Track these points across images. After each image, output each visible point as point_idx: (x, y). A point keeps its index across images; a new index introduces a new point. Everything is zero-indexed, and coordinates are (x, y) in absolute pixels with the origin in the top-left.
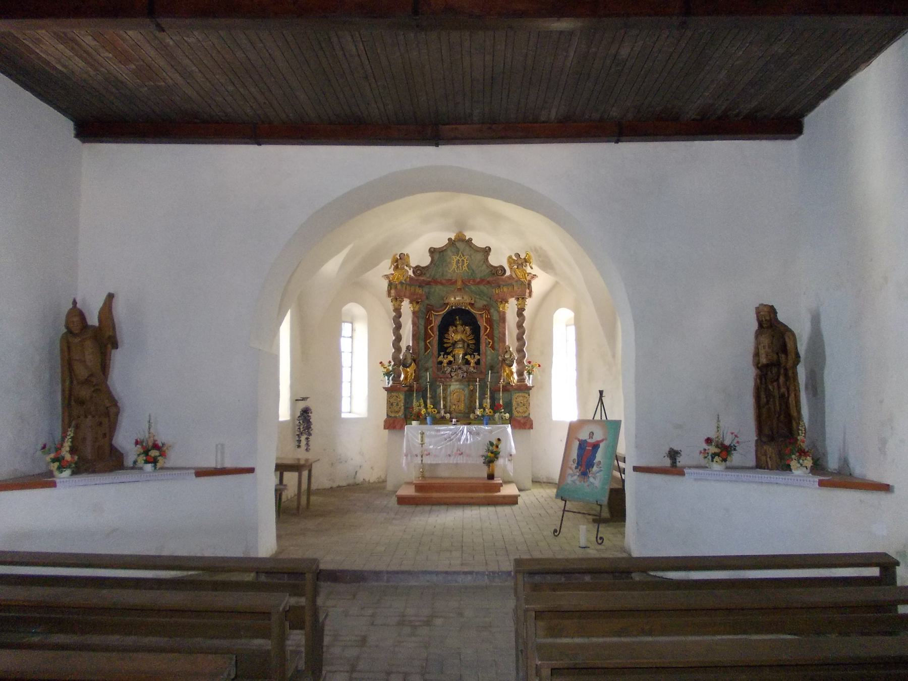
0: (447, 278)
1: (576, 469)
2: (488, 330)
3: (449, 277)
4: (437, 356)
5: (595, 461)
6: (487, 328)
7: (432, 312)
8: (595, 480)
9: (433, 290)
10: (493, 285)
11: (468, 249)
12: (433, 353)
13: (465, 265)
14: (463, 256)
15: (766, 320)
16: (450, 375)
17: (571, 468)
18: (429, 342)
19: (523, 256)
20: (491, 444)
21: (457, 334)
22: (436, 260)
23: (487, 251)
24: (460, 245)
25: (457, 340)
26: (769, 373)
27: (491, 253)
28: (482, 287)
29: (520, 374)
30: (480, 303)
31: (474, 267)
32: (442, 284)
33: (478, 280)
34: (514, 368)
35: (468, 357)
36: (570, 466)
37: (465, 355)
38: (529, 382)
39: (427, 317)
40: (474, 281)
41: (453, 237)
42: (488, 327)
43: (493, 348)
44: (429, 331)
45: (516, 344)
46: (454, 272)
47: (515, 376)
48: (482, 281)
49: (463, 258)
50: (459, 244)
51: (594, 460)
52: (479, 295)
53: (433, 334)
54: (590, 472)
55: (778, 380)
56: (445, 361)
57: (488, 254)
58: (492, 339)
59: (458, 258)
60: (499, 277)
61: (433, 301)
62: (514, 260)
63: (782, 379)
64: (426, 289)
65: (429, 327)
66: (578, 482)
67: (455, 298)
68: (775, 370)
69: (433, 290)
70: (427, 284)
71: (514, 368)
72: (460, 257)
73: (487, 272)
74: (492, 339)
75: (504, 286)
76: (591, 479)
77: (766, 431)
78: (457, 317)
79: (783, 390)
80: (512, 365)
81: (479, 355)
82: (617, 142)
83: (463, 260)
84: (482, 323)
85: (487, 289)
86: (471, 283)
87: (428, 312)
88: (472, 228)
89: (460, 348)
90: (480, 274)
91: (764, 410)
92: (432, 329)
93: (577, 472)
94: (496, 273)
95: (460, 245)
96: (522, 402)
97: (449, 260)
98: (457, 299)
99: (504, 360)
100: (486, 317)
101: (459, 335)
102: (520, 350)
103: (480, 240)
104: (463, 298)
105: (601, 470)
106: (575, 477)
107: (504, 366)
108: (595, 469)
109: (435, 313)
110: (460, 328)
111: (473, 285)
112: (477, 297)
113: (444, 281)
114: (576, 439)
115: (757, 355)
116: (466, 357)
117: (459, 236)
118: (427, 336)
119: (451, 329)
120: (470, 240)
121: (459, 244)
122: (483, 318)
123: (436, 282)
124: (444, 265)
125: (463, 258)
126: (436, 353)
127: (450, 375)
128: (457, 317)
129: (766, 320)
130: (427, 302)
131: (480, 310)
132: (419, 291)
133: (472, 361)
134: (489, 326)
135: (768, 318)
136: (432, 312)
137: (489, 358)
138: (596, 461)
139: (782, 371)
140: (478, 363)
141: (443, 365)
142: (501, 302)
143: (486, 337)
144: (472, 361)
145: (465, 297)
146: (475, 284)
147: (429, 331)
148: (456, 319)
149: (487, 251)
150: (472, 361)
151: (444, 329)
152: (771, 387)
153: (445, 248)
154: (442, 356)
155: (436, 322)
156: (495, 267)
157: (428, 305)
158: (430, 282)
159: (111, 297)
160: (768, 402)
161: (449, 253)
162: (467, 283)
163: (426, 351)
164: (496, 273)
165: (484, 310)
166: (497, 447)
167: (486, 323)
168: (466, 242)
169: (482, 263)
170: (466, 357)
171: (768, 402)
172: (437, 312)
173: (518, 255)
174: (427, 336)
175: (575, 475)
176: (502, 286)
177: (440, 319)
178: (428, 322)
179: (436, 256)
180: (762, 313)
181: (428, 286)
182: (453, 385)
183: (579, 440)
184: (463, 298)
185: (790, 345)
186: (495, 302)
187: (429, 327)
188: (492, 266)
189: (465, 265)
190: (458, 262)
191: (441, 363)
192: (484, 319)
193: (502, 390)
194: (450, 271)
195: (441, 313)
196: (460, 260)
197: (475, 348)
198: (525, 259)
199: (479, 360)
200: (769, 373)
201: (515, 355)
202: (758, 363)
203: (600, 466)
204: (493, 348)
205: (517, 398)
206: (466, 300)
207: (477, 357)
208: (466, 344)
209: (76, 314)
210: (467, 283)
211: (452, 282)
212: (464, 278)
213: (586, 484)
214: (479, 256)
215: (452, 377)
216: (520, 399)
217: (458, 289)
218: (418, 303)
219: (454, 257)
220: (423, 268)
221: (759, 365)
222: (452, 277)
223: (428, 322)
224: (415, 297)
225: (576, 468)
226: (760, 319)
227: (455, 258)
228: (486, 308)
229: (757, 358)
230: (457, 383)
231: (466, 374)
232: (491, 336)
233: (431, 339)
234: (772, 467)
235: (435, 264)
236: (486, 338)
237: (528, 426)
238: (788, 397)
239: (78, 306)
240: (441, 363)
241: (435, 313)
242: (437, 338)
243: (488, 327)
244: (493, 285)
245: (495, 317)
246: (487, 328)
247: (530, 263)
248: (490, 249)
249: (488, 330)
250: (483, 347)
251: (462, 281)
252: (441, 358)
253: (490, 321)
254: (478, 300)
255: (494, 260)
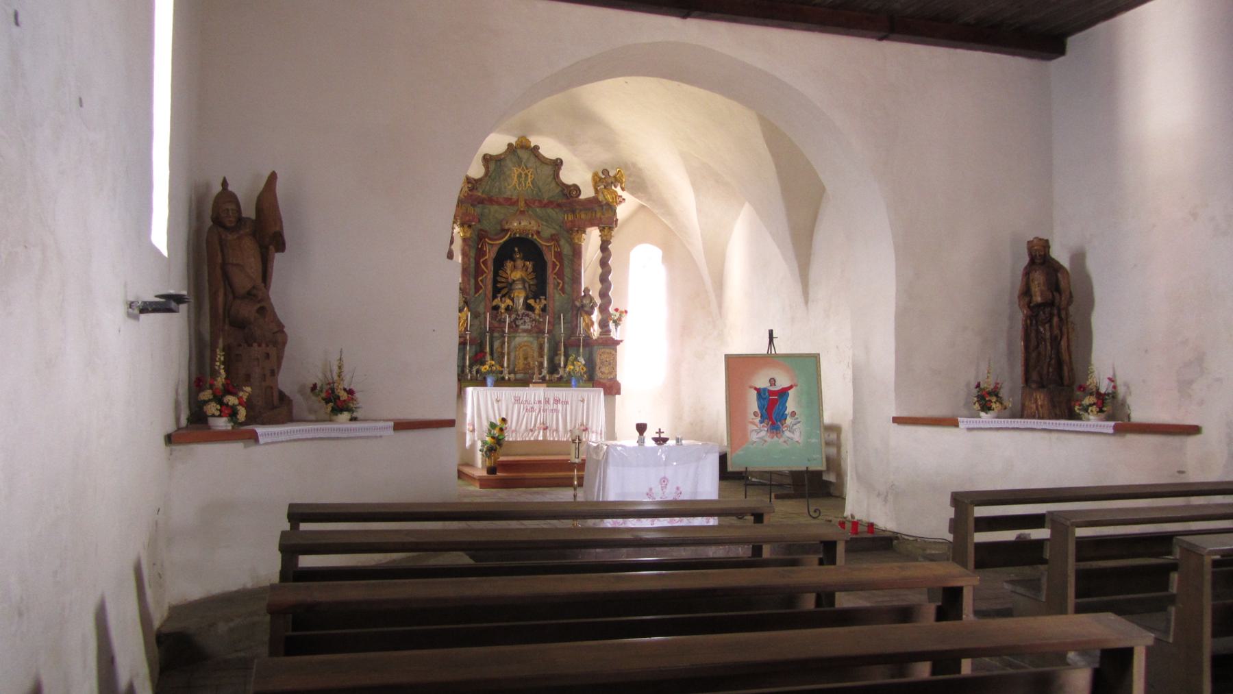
0: (505, 196)
1: (761, 423)
2: (558, 267)
3: (508, 194)
4: (491, 299)
5: (786, 412)
6: (557, 265)
7: (486, 240)
8: (793, 433)
9: (486, 211)
10: (564, 209)
11: (533, 159)
12: (486, 295)
13: (529, 180)
14: (527, 169)
15: (1040, 256)
16: (515, 324)
17: (753, 423)
18: (482, 281)
19: (612, 173)
20: (493, 425)
21: (517, 272)
22: (491, 172)
23: (557, 164)
24: (523, 154)
25: (515, 279)
26: (1041, 313)
27: (563, 168)
28: (549, 211)
29: (604, 325)
30: (547, 232)
31: (540, 184)
32: (498, 203)
33: (546, 201)
34: (596, 317)
35: (531, 302)
36: (751, 420)
37: (526, 298)
38: (615, 334)
39: (480, 246)
40: (540, 201)
41: (513, 140)
42: (557, 263)
43: (563, 290)
44: (482, 265)
45: (599, 286)
46: (515, 190)
47: (596, 326)
48: (550, 204)
49: (527, 171)
50: (522, 151)
51: (786, 410)
52: (547, 221)
53: (487, 269)
54: (783, 425)
55: (1050, 321)
56: (503, 306)
57: (559, 169)
58: (562, 280)
59: (520, 170)
60: (574, 199)
61: (486, 225)
62: (601, 179)
63: (1055, 320)
64: (479, 209)
65: (482, 260)
66: (768, 439)
67: (520, 223)
68: (1047, 310)
69: (486, 211)
70: (479, 203)
71: (596, 317)
72: (523, 170)
73: (557, 191)
74: (562, 280)
75: (581, 210)
76: (787, 434)
77: (1035, 376)
78: (516, 249)
79: (1056, 331)
80: (592, 313)
81: (545, 299)
82: (881, 39)
83: (526, 175)
84: (550, 258)
85: (557, 213)
86: (536, 204)
87: (481, 240)
88: (540, 132)
89: (519, 289)
90: (550, 192)
91: (1034, 355)
92: (485, 263)
93: (763, 426)
94: (570, 194)
95: (523, 154)
96: (608, 360)
97: (508, 173)
98: (523, 224)
99: (583, 306)
100: (556, 249)
101: (519, 272)
102: (604, 294)
103: (549, 148)
104: (530, 223)
105: (799, 422)
106: (763, 433)
107: (583, 314)
108: (789, 421)
109: (491, 242)
110: (519, 263)
111: (538, 207)
112: (545, 223)
113: (501, 200)
114: (751, 387)
115: (1026, 292)
116: (528, 301)
117: (522, 142)
118: (478, 272)
119: (509, 264)
120: (536, 148)
121: (522, 151)
122: (551, 252)
123: (491, 201)
124: (502, 178)
125: (527, 171)
126: (490, 295)
127: (515, 324)
128: (516, 249)
129: (1040, 256)
130: (479, 226)
131: (548, 240)
132: (471, 210)
133: (538, 307)
134: (559, 262)
135: (1042, 253)
136: (486, 240)
137: (557, 304)
138: (788, 411)
139: (1055, 312)
140: (544, 310)
141: (500, 310)
142: (577, 231)
143: (554, 276)
144: (538, 308)
145: (533, 222)
146: (542, 207)
147: (482, 265)
148: (515, 252)
149: (557, 164)
150: (538, 308)
151: (499, 263)
152: (1042, 329)
153: (503, 156)
154: (499, 299)
155: (491, 254)
156: (568, 186)
157: (481, 230)
158: (484, 199)
159: (273, 177)
160: (1037, 346)
161: (509, 163)
162: (534, 203)
163: (476, 293)
164: (570, 194)
165: (553, 240)
166: (501, 430)
167: (555, 258)
168: (531, 150)
169: (550, 179)
170: (528, 301)
171: (1037, 346)
172: (491, 239)
173: (605, 172)
174: (478, 272)
175: (761, 431)
176: (577, 211)
177: (495, 249)
178: (480, 253)
179: (492, 166)
180: (1036, 248)
181: (480, 206)
182: (519, 336)
183: (756, 389)
184: (530, 223)
185: (1063, 284)
186: (568, 232)
187: (482, 260)
188: (564, 184)
189: (529, 180)
190: (520, 176)
191: (496, 308)
192: (553, 252)
193: (583, 345)
194: (510, 187)
195: (498, 242)
196: (523, 173)
197: (538, 289)
198: (615, 177)
199: (545, 305)
200: (1041, 313)
201: (598, 301)
202: (1030, 302)
203: (796, 417)
204: (563, 290)
205: (600, 355)
206: (533, 227)
207: (544, 302)
208: (527, 285)
209: (226, 196)
210: (531, 205)
211: (510, 202)
212: (527, 198)
213: (781, 440)
214: (547, 170)
215: (517, 326)
216: (604, 357)
217: (521, 211)
218: (470, 226)
219: (515, 169)
220: (475, 180)
221: (1032, 305)
222: (512, 196)
223: (480, 253)
224: (467, 218)
225: (761, 422)
226: (1034, 254)
227: (516, 171)
228: (554, 238)
229: (1027, 299)
230: (525, 334)
231: (534, 322)
232: (560, 275)
233: (484, 276)
234: (1043, 415)
235: (490, 177)
236: (554, 278)
237: (615, 391)
238: (1061, 340)
239: (230, 188)
240: (496, 308)
241: (491, 242)
242: (491, 276)
243: (557, 263)
244: (564, 209)
245: (566, 250)
246: (557, 265)
247: (621, 184)
248: (561, 162)
249: (558, 267)
250: (550, 288)
251: (526, 203)
252: (497, 302)
253: (559, 255)
254: (545, 228)
255: (567, 176)
